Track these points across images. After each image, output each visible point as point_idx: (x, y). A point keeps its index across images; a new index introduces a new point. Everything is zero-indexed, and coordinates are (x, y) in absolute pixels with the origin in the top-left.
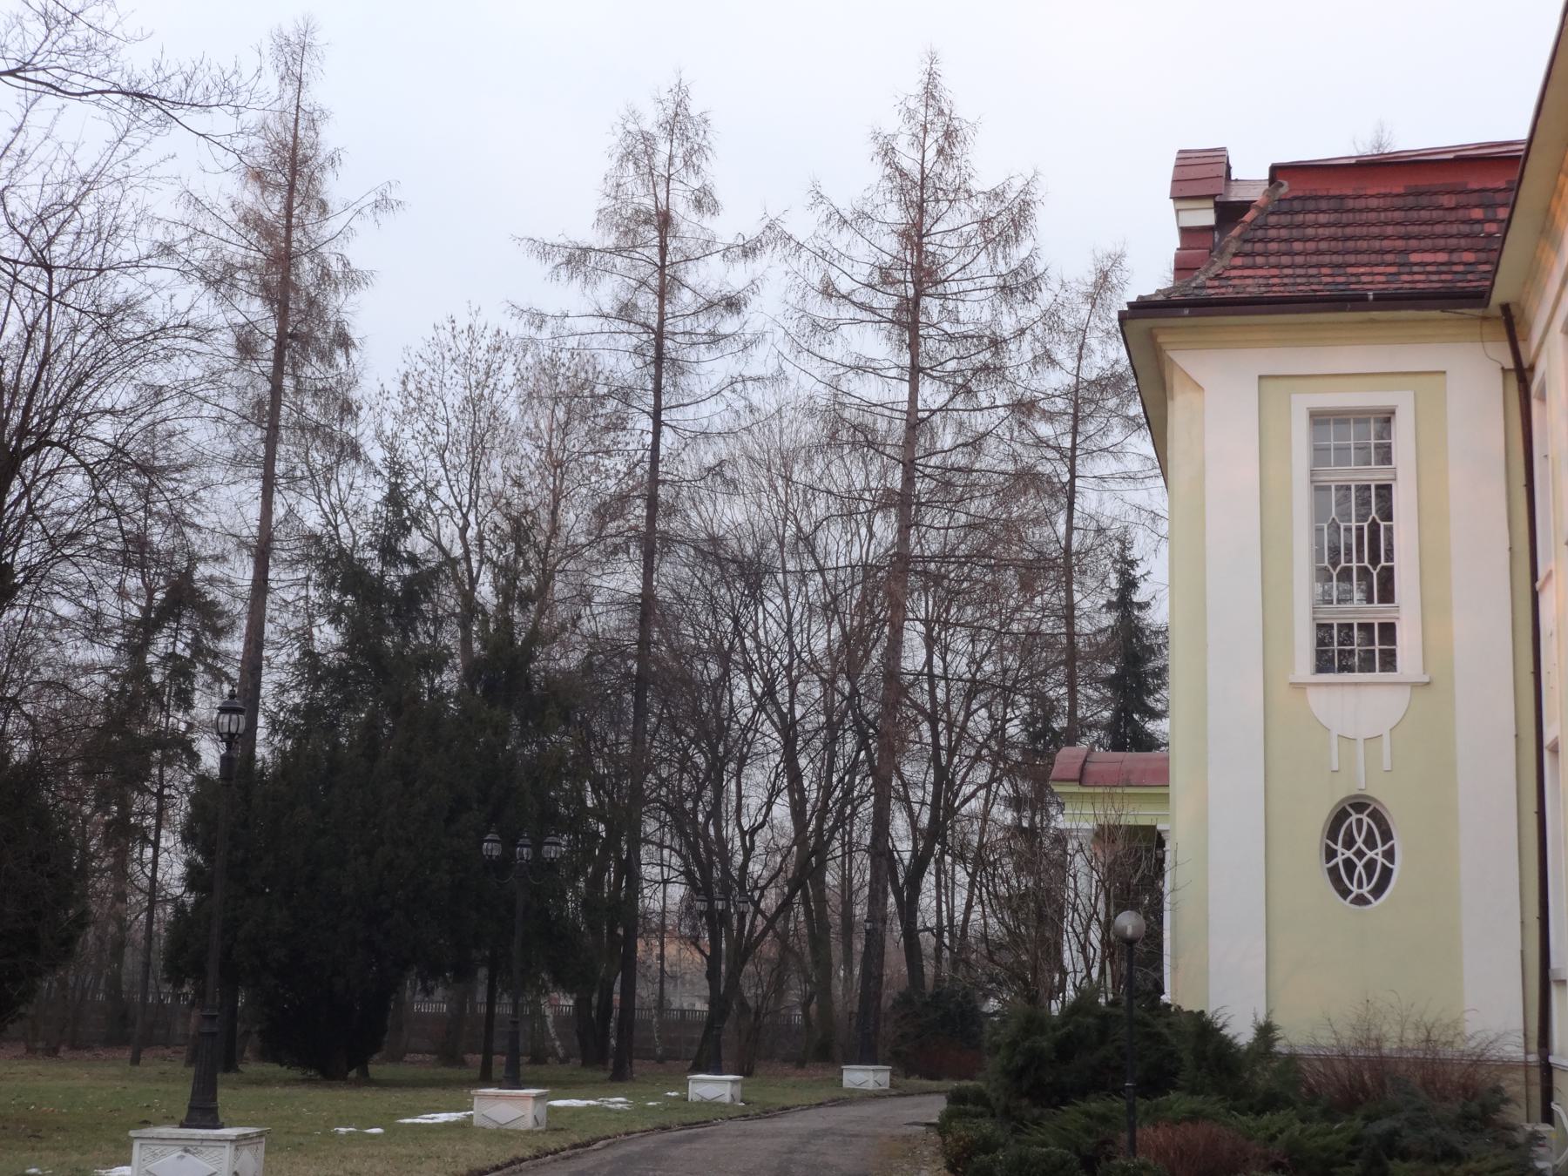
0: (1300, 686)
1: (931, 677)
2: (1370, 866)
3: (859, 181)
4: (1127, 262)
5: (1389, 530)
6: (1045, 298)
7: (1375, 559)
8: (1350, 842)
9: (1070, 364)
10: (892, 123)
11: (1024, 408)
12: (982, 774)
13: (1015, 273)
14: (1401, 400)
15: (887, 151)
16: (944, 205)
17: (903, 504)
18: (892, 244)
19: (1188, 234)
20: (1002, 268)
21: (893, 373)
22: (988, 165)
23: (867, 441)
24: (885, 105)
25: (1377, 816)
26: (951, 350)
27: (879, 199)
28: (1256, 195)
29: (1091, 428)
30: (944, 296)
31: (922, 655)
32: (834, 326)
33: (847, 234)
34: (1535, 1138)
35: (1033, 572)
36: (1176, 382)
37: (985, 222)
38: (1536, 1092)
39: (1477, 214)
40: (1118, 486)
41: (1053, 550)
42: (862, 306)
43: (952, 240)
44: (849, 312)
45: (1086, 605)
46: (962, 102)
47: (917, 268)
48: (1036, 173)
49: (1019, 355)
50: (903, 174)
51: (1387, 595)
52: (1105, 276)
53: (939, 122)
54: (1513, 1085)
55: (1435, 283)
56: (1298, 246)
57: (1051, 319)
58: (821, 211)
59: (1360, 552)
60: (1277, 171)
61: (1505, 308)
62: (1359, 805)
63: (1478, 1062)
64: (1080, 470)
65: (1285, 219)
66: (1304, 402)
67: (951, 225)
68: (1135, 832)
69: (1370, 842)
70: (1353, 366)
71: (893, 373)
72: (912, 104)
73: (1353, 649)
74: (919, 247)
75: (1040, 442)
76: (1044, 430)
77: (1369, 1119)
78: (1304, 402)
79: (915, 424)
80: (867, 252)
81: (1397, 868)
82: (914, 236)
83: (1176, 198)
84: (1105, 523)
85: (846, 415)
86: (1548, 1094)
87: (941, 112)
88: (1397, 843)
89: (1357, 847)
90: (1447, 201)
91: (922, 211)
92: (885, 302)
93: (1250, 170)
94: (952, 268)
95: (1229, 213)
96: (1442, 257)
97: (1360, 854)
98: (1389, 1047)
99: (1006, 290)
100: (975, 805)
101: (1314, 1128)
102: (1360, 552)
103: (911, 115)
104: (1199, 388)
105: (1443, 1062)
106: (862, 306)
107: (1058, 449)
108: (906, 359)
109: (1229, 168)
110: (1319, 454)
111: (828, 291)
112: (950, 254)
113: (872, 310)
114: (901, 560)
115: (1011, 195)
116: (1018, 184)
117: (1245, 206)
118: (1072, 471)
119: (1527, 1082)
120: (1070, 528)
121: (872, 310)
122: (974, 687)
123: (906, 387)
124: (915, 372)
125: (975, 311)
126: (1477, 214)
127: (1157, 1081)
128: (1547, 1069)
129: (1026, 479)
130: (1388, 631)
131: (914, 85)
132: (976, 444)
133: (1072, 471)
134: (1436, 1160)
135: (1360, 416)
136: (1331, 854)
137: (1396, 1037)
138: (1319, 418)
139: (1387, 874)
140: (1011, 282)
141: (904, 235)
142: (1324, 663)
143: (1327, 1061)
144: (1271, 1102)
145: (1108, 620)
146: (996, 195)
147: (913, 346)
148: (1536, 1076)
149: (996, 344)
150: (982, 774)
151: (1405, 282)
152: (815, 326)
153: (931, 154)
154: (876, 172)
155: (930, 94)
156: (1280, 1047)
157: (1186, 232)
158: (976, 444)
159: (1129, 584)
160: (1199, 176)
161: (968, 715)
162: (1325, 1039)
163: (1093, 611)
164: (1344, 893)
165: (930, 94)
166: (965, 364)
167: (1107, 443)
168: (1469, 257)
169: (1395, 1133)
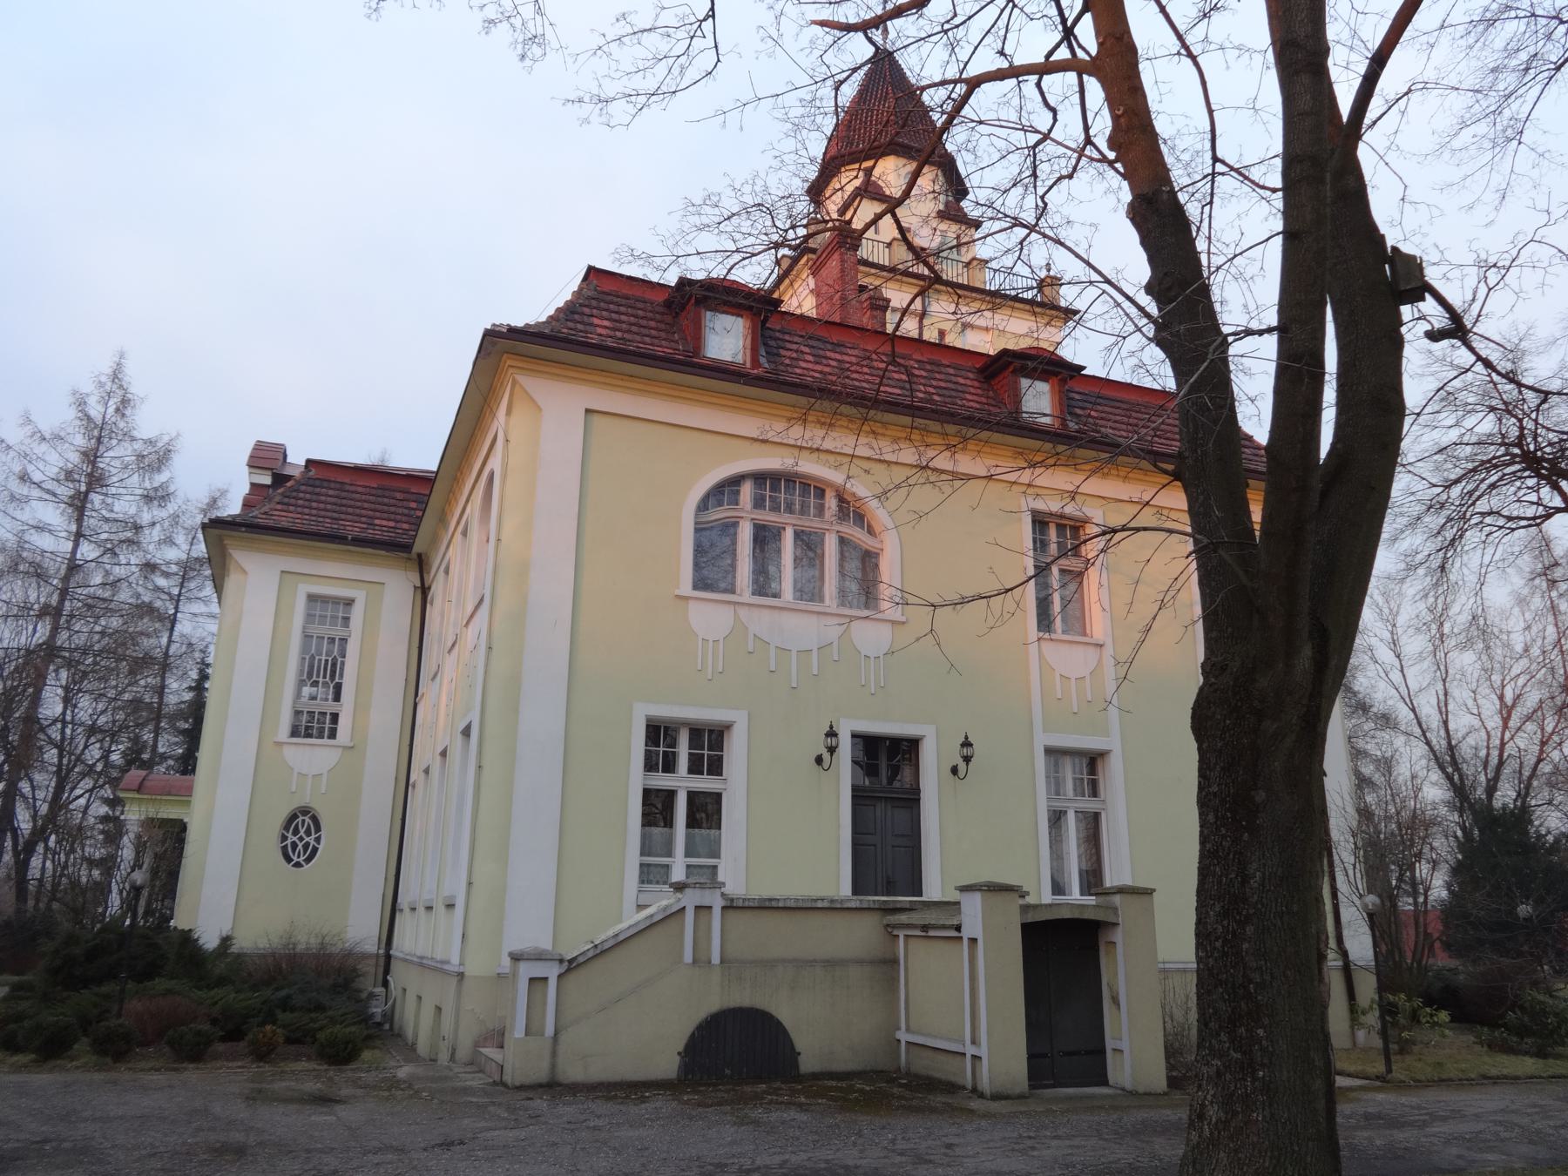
0: (279, 744)
1: (64, 723)
2: (306, 846)
3: (58, 415)
4: (229, 496)
5: (343, 663)
6: (171, 508)
7: (333, 677)
8: (296, 832)
9: (185, 547)
10: (87, 387)
11: (150, 567)
12: (87, 783)
13: (156, 489)
14: (359, 595)
15: (81, 403)
16: (114, 442)
17: (51, 612)
18: (75, 458)
19: (255, 486)
20: (147, 485)
21: (64, 534)
22: (147, 423)
23: (39, 574)
24: (87, 372)
25: (315, 819)
26: (106, 527)
27: (70, 430)
28: (296, 473)
29: (192, 585)
30: (106, 495)
31: (59, 709)
32: (27, 499)
33: (44, 447)
34: (372, 995)
35: (142, 663)
36: (232, 567)
37: (140, 457)
38: (381, 970)
39: (414, 505)
40: (198, 621)
41: (158, 653)
42: (48, 491)
43: (117, 463)
44: (36, 493)
45: (175, 686)
46: (137, 384)
47: (90, 475)
48: (179, 435)
49: (152, 536)
50: (89, 418)
51: (337, 698)
52: (214, 501)
53: (121, 393)
54: (368, 968)
55: (386, 536)
56: (314, 505)
57: (175, 518)
58: (28, 430)
59: (324, 670)
60: (309, 462)
61: (419, 555)
62: (305, 811)
63: (349, 954)
64: (181, 608)
65: (310, 489)
66: (304, 589)
67: (115, 457)
68: (165, 823)
69: (308, 833)
70: (334, 573)
71: (64, 534)
72: (103, 379)
73: (314, 725)
74: (94, 463)
75: (158, 589)
76: (162, 582)
77: (277, 989)
78: (304, 589)
79: (73, 567)
80: (52, 462)
81: (321, 847)
82: (91, 456)
83: (250, 466)
84: (194, 641)
85: (25, 554)
86: (387, 971)
87: (121, 387)
88: (323, 833)
89: (300, 834)
90: (399, 495)
91: (99, 440)
92: (65, 491)
93: (297, 458)
94: (115, 479)
95: (280, 479)
96: (392, 524)
97: (301, 839)
98: (301, 948)
99: (148, 499)
100: (82, 801)
101: (242, 996)
102: (324, 670)
103: (101, 385)
104: (245, 572)
105: (330, 955)
106: (48, 491)
107: (169, 594)
108: (74, 528)
109: (285, 456)
110: (309, 617)
111: (24, 477)
112: (114, 471)
113: (54, 495)
114: (49, 651)
115: (160, 445)
116: (166, 439)
117: (289, 478)
118: (176, 608)
119: (377, 965)
120: (170, 641)
121: (54, 495)
122: (92, 730)
123: (70, 545)
124: (79, 536)
125: (125, 506)
126: (414, 505)
127: (149, 972)
128: (388, 957)
129: (148, 610)
130: (335, 717)
131: (106, 368)
132: (115, 584)
133: (176, 608)
134: (310, 1011)
135: (336, 601)
136: (284, 838)
137: (305, 940)
138: (312, 598)
139: (315, 850)
140: (152, 494)
141: (85, 454)
142: (295, 732)
143: (264, 956)
144: (221, 981)
145: (188, 696)
146: (150, 442)
147: (79, 521)
148: (382, 961)
149: (137, 528)
150: (87, 783)
151: (370, 533)
152: (13, 498)
153: (111, 410)
154: (71, 413)
155: (116, 376)
156: (234, 949)
157: (253, 485)
158: (115, 584)
159: (204, 677)
160: (266, 457)
161: (86, 747)
162: (263, 944)
163: (178, 691)
164: (289, 860)
165: (116, 376)
166: (112, 537)
167: (201, 595)
168: (406, 526)
169: (289, 997)
